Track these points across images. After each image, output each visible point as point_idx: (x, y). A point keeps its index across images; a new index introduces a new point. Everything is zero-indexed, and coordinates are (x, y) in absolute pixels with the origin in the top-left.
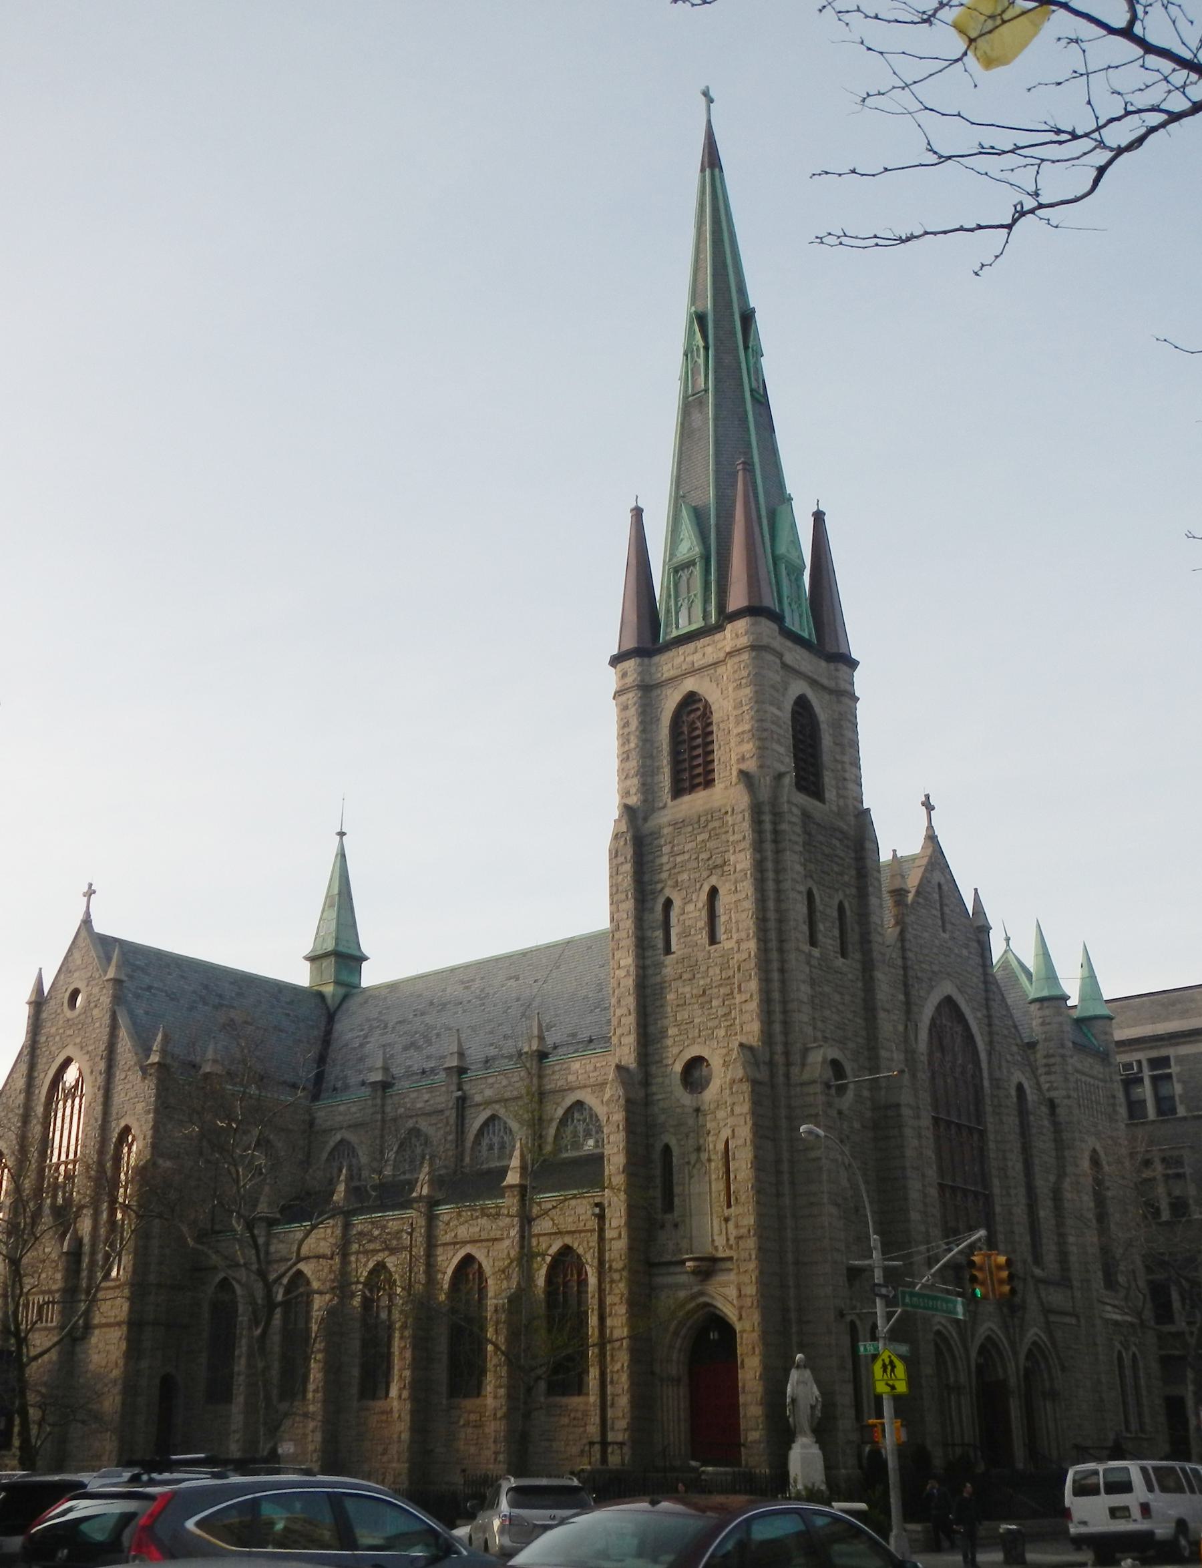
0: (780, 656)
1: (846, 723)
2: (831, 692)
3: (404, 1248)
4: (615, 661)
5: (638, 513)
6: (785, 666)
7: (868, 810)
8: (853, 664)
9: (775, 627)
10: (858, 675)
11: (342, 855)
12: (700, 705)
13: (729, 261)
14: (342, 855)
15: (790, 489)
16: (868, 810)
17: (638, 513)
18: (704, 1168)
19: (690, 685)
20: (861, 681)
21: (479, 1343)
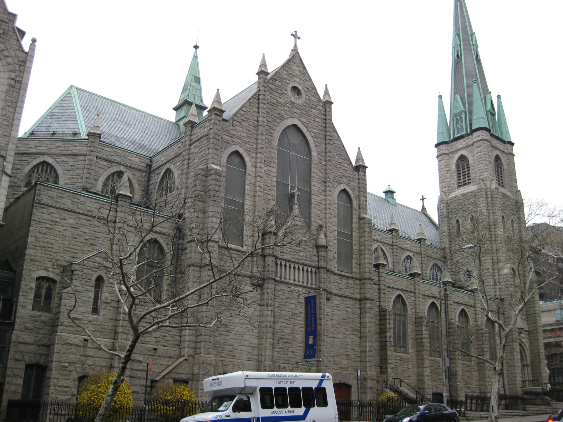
0: (490, 142)
1: (512, 164)
2: (506, 154)
3: (207, 265)
4: (436, 146)
5: (440, 97)
6: (492, 146)
7: (520, 191)
8: (512, 144)
9: (488, 133)
10: (515, 157)
11: (195, 57)
12: (465, 159)
13: (466, 17)
14: (195, 57)
15: (490, 90)
16: (520, 191)
17: (440, 97)
18: (497, 325)
19: (462, 152)
20: (516, 150)
21: (45, 299)
